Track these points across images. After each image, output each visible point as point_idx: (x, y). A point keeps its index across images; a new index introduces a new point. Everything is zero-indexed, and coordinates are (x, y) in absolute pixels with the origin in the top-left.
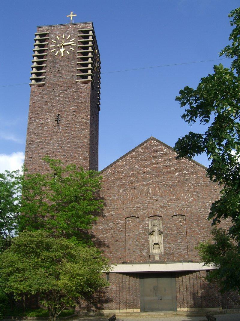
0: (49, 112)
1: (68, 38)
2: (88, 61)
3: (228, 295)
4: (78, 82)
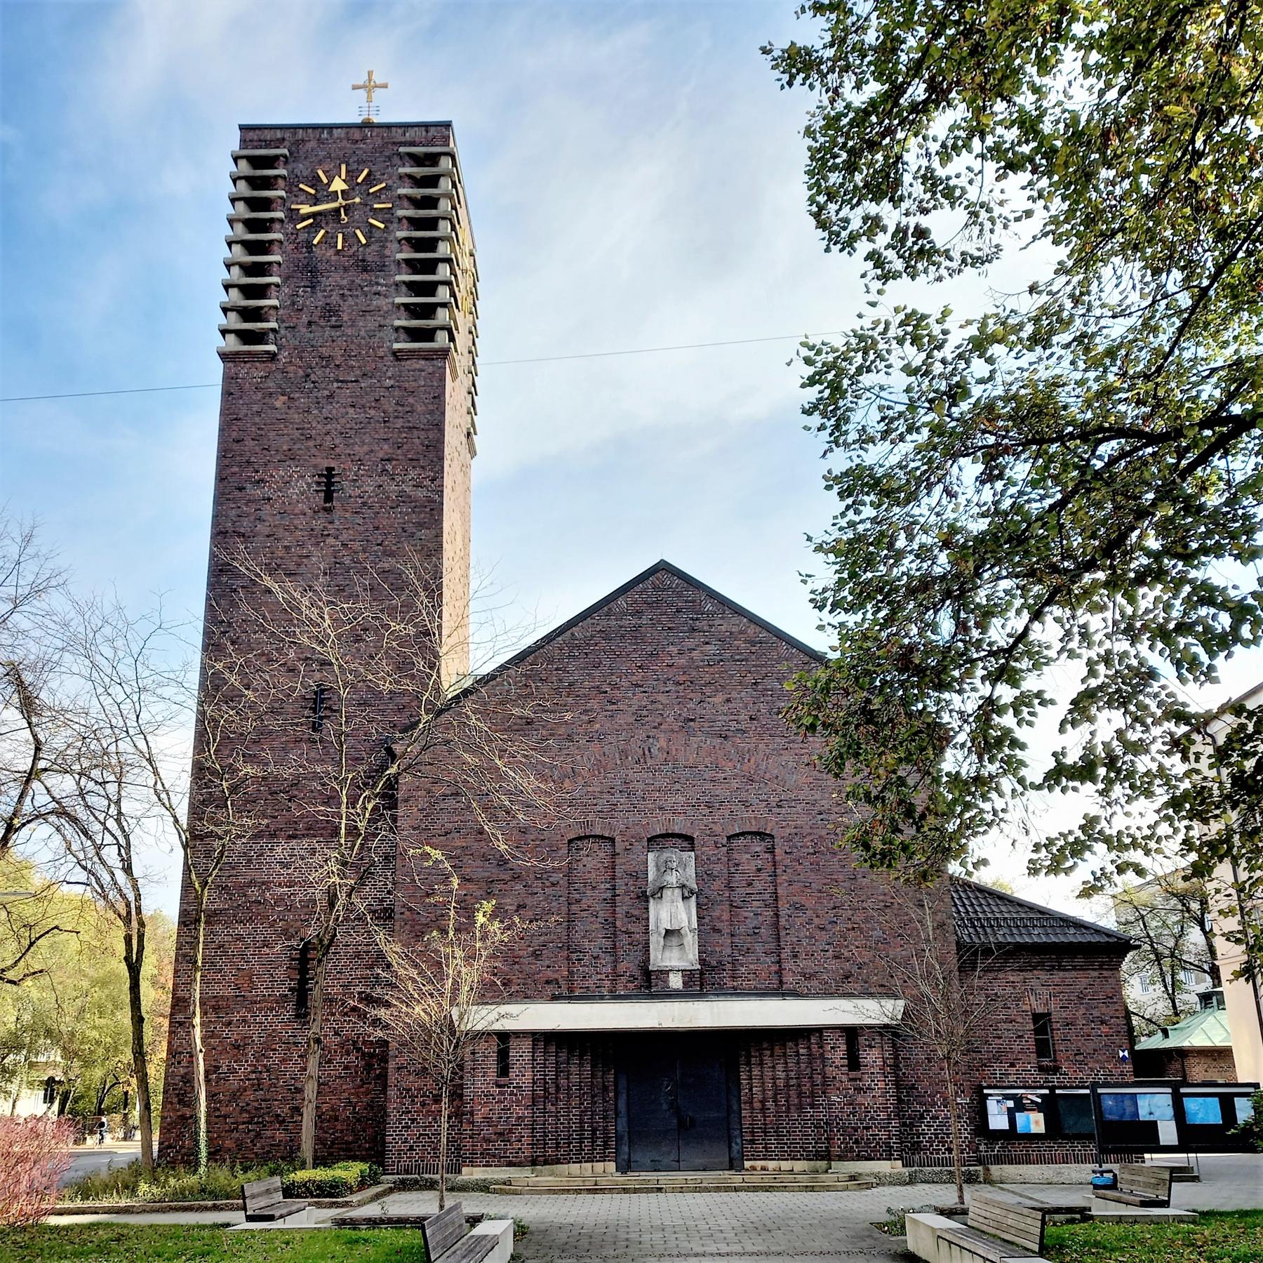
0: (291, 456)
1: (360, 180)
2: (434, 273)
3: (922, 1117)
4: (400, 350)
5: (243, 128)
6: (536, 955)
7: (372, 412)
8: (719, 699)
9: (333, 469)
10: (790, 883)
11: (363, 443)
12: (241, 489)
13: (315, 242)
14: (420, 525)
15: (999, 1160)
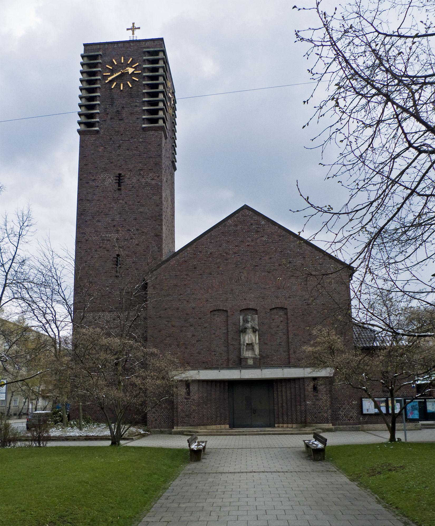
0: (105, 170)
5: (85, 45)
6: (199, 353)
7: (135, 152)
8: (268, 257)
9: (121, 174)
10: (293, 326)
11: (132, 164)
12: (87, 183)
13: (113, 87)
14: (154, 194)
15: (367, 423)
